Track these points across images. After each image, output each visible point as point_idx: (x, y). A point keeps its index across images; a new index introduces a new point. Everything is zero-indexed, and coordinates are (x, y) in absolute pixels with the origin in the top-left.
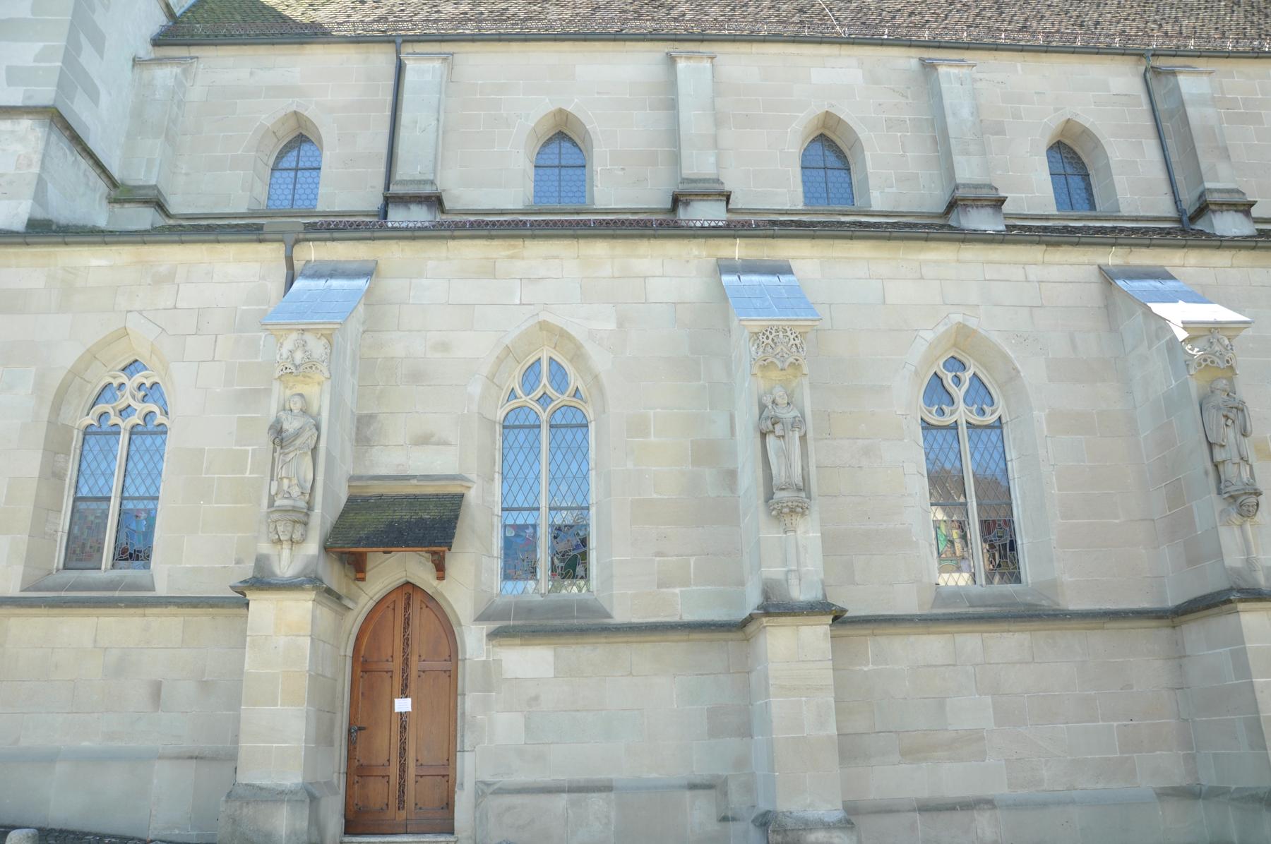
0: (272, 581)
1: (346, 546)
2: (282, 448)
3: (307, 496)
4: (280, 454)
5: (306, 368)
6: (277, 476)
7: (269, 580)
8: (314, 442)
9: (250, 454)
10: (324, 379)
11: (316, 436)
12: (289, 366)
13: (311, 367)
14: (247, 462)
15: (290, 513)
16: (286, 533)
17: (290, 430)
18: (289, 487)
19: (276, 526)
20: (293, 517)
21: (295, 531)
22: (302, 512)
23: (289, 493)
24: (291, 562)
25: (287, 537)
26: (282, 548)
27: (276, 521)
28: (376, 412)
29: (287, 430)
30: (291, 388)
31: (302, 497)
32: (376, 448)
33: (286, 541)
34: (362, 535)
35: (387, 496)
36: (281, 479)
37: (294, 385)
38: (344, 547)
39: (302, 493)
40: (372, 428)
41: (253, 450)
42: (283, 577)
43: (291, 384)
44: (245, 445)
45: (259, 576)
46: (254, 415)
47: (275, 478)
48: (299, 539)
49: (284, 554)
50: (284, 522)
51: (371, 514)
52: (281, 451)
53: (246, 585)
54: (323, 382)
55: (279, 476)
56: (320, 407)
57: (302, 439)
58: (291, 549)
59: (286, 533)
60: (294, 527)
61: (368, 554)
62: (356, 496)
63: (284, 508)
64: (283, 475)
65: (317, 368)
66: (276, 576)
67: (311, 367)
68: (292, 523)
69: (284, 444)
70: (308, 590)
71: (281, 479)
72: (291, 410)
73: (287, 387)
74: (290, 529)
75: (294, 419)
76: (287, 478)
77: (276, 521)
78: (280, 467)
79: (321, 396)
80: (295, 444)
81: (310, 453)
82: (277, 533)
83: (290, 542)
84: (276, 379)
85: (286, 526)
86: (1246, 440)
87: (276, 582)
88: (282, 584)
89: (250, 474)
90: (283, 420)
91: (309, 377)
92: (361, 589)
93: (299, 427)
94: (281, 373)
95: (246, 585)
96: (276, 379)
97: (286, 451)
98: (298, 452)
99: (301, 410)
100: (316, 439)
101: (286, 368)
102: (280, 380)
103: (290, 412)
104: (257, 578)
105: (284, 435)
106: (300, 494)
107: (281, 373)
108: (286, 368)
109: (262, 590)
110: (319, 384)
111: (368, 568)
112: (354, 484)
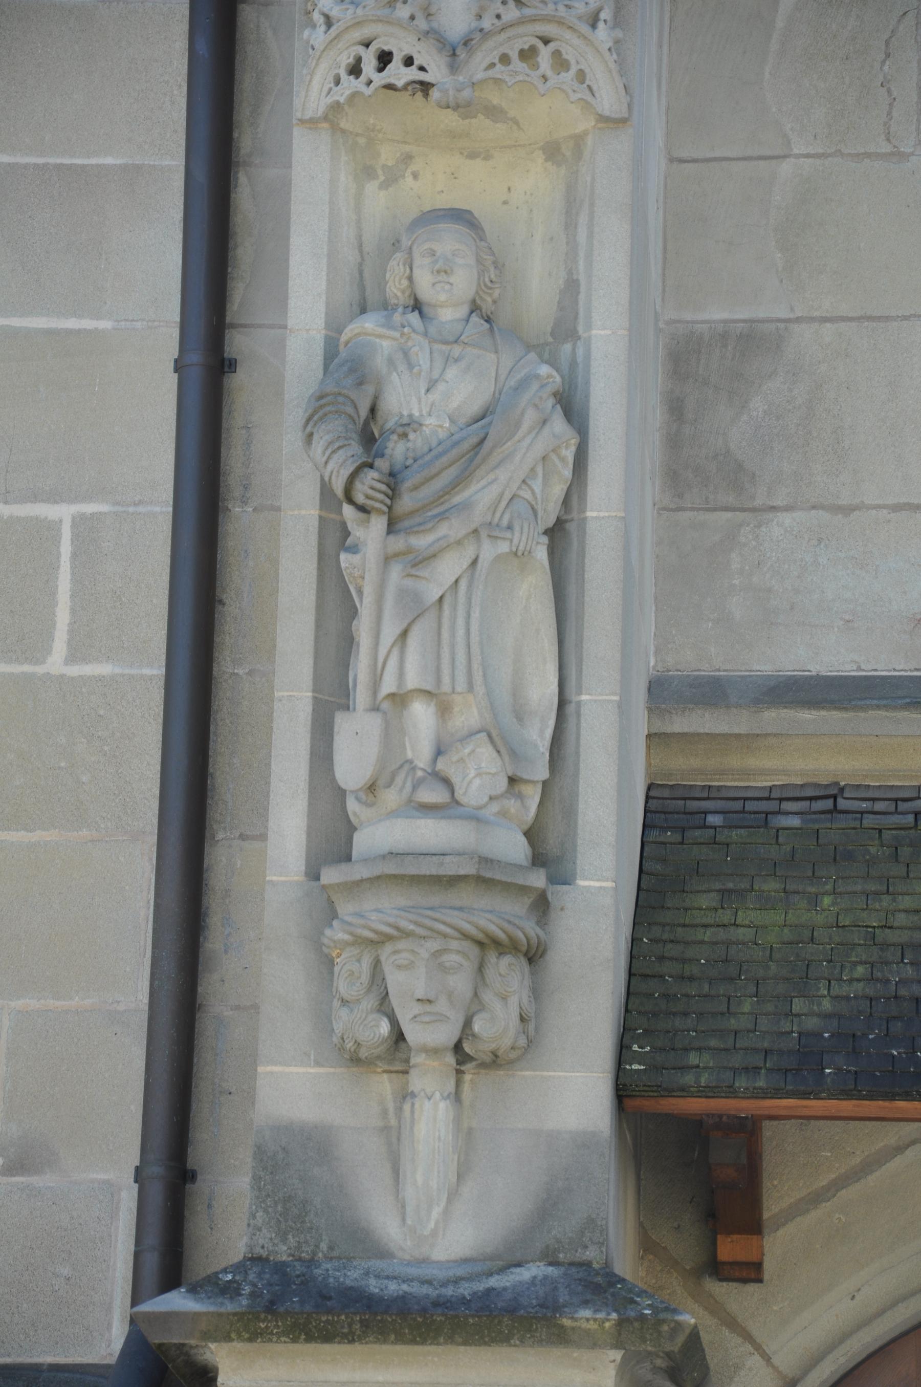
0: (373, 1286)
1: (741, 1083)
2: (392, 527)
3: (533, 796)
4: (388, 560)
5: (505, 59)
6: (375, 692)
7: (352, 1276)
8: (558, 490)
9: (66, 548)
10: (586, 124)
11: (573, 449)
12: (400, 46)
13: (528, 55)
14: (52, 594)
15: (466, 896)
16: (442, 1006)
17: (430, 421)
18: (439, 752)
19: (377, 964)
20: (482, 923)
21: (488, 997)
22: (524, 889)
23: (447, 782)
24: (461, 1177)
25: (446, 1034)
26: (405, 1095)
27: (383, 939)
28: (783, 314)
29: (407, 427)
30: (392, 179)
31: (512, 805)
32: (787, 519)
33: (434, 1052)
34: (812, 1023)
35: (861, 790)
36: (400, 699)
37: (408, 158)
38: (732, 1093)
39: (512, 780)
40: (757, 405)
41: (79, 521)
42: (424, 1261)
43: (387, 155)
44: (35, 498)
45: (283, 1253)
46: (72, 323)
47: (361, 697)
48: (507, 1042)
49: (422, 1130)
50: (434, 945)
51: (814, 900)
52: (398, 543)
53: (229, 1307)
54: (579, 140)
55: (388, 685)
56: (571, 287)
57: (503, 475)
58: (457, 1097)
59: (442, 1006)
60: (481, 968)
61: (766, 1124)
62: (686, 794)
63: (428, 868)
64: (412, 681)
65: (560, 63)
66: (383, 1253)
67: (528, 55)
68: (474, 951)
69: (406, 502)
70: (591, 1341)
71: (400, 699)
72: (417, 306)
73: (368, 172)
74: (461, 983)
75: (448, 360)
76: (428, 694)
77: (383, 939)
78: (390, 632)
79: (570, 225)
80: (466, 506)
81: (541, 554)
82: (384, 1006)
83: (451, 1059)
84: (311, 123)
85: (444, 969)
86: (503, 17)
87: (393, 1288)
88: (436, 1304)
89: (72, 658)
90: (379, 362)
91: (494, 113)
92: (748, 1337)
93: (475, 408)
94: (350, 84)
95: (229, 1307)
96: (311, 123)
97: (421, 542)
98: (488, 551)
99: (475, 308)
100: (568, 473)
101: (385, 59)
102: (335, 128)
103: (414, 318)
104: (280, 1268)
105: (397, 450)
106: (503, 783)
107: (341, 94)
108: (385, 59)
109: (327, 1337)
110: (552, 151)
111: (771, 1208)
112: (680, 724)
